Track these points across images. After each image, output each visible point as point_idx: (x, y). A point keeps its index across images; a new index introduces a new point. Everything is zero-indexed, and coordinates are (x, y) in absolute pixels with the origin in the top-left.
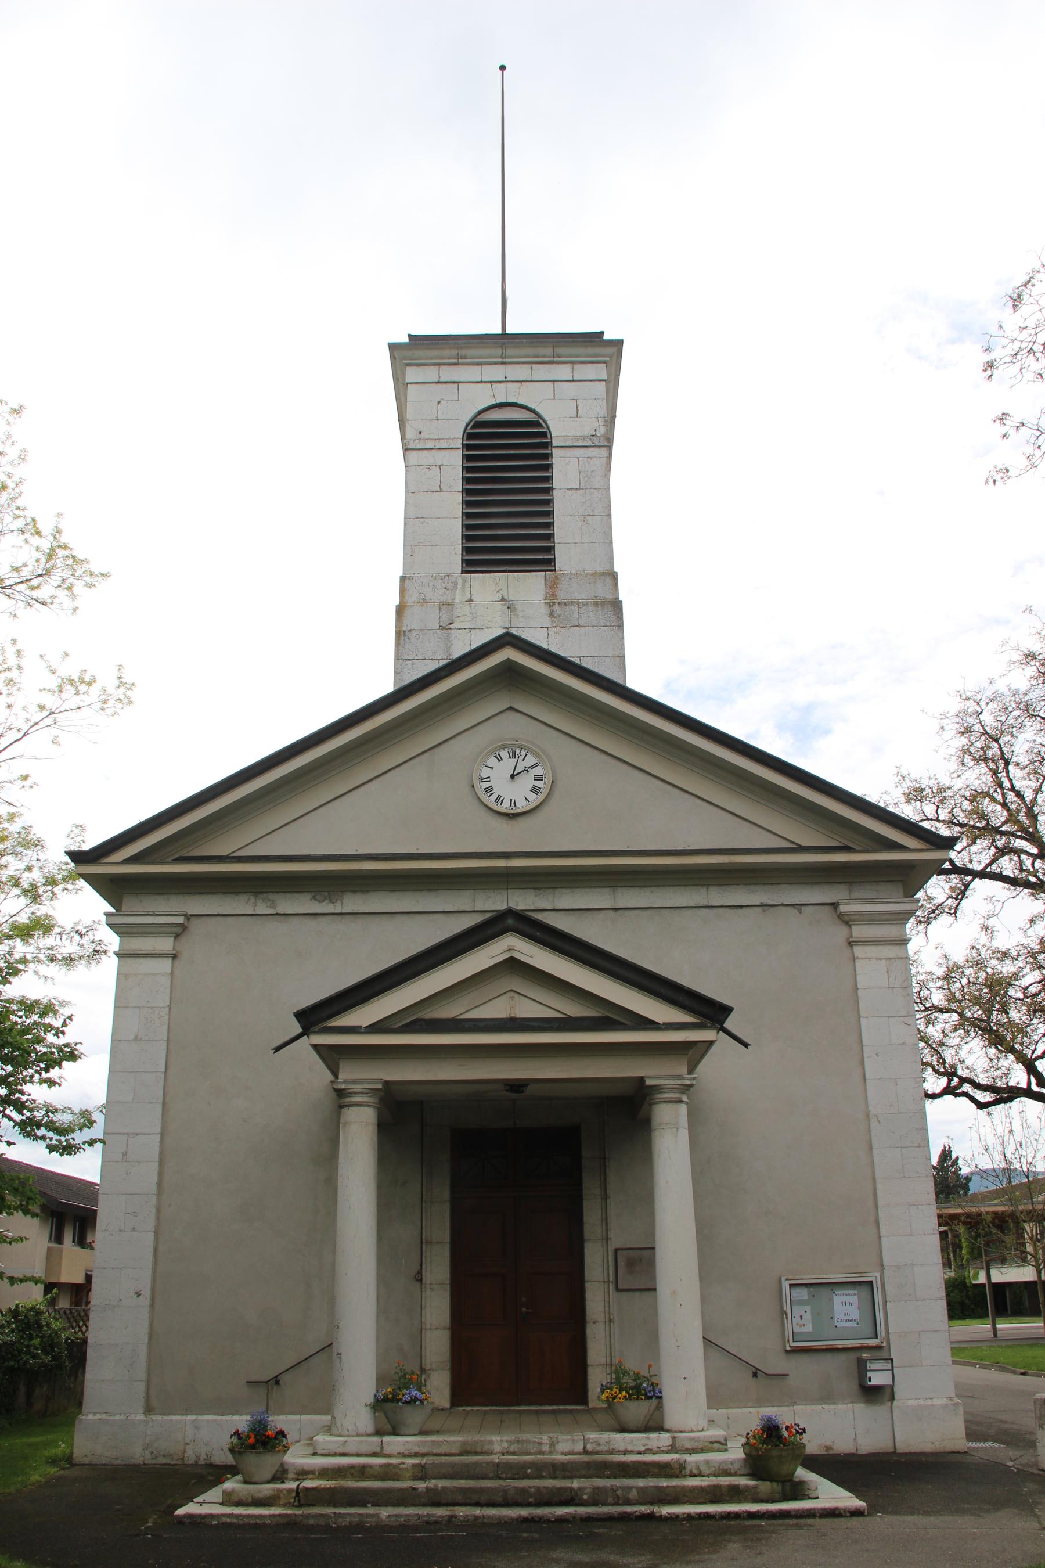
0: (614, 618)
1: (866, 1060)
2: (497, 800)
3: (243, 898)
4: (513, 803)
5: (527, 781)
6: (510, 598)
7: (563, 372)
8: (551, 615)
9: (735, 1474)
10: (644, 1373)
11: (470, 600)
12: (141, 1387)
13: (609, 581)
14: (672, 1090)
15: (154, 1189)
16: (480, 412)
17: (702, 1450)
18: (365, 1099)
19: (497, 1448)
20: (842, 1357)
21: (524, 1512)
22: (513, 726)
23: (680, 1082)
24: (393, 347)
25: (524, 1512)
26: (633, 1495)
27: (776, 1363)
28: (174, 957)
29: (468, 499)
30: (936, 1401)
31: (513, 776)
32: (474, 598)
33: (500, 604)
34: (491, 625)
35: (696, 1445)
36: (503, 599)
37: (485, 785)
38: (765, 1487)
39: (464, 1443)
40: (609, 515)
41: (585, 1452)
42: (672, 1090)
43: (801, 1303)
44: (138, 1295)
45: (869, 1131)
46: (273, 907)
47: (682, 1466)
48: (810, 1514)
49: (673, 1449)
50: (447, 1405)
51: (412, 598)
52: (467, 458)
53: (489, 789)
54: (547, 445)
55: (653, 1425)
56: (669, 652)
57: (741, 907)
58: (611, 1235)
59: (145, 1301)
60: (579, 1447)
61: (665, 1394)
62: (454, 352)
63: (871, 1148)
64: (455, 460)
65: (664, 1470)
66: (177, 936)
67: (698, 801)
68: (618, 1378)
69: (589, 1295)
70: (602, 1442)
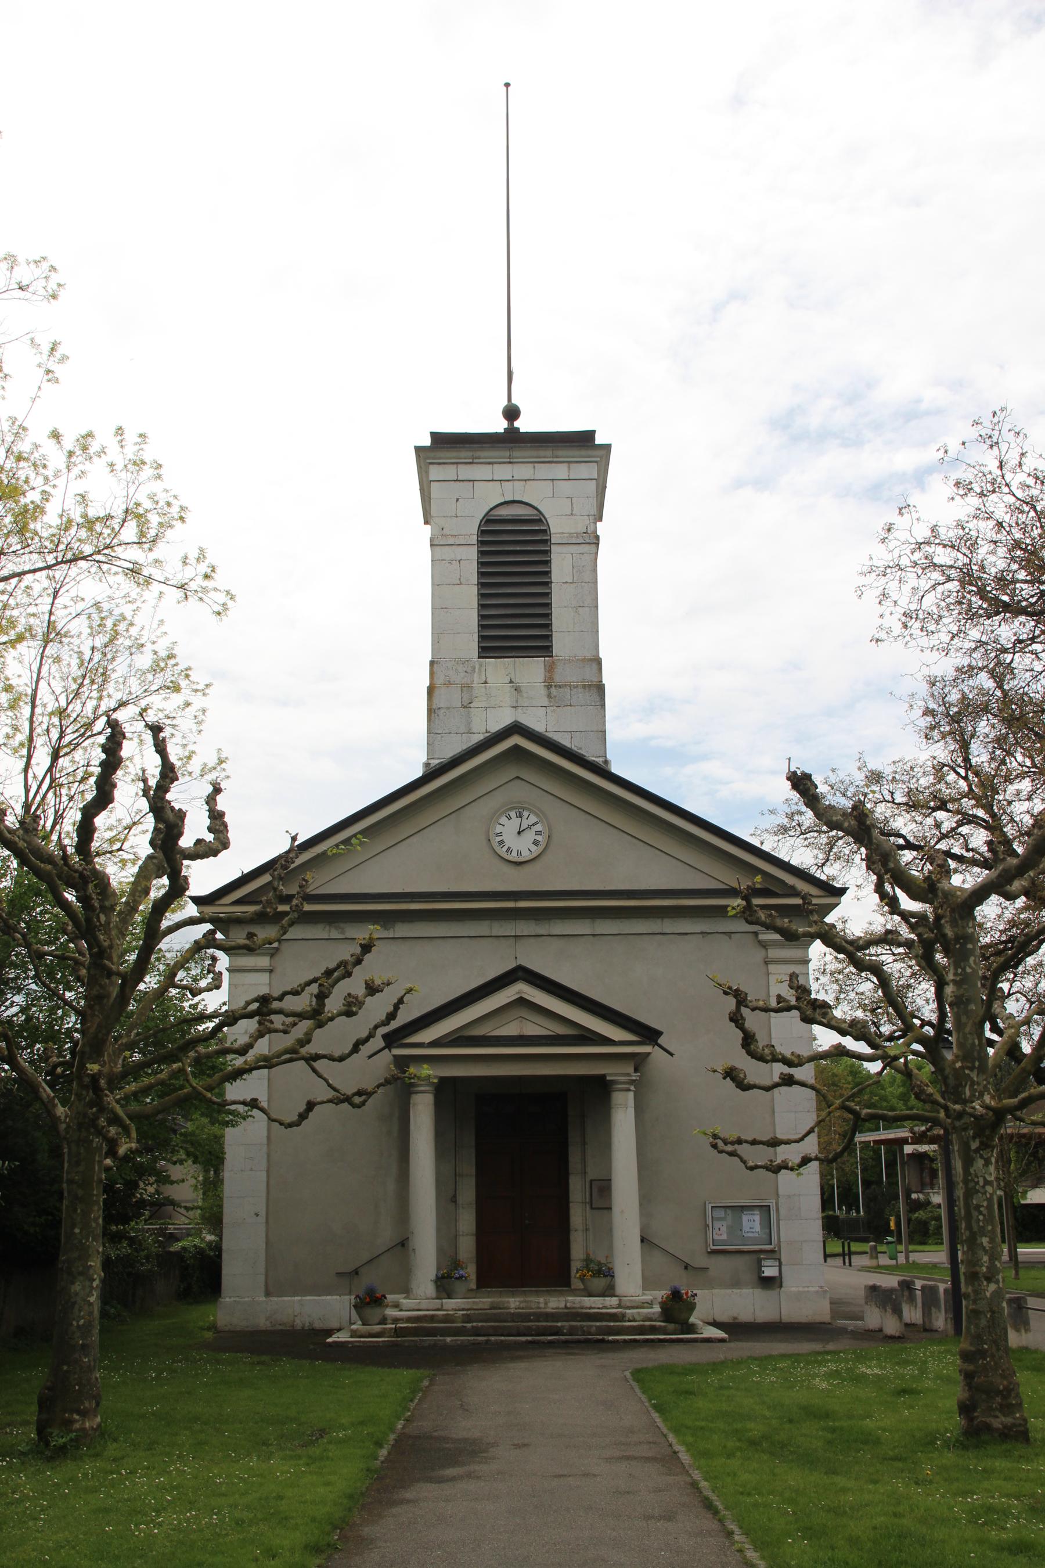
0: (598, 699)
2: (507, 851)
3: (320, 926)
4: (519, 853)
5: (530, 836)
6: (517, 680)
7: (560, 471)
8: (549, 696)
9: (655, 1321)
10: (603, 1261)
11: (486, 683)
12: (262, 1278)
13: (595, 666)
15: (265, 1141)
17: (637, 1307)
18: (427, 1088)
19: (512, 1306)
20: (747, 1257)
21: (530, 1338)
22: (518, 792)
24: (419, 450)
25: (530, 1338)
26: (593, 1329)
28: (271, 971)
29: (483, 592)
30: (811, 1289)
31: (519, 833)
32: (489, 680)
33: (510, 694)
34: (502, 704)
35: (634, 1304)
36: (511, 682)
37: (499, 839)
38: (671, 1326)
39: (492, 1303)
40: (597, 607)
41: (566, 1307)
43: (720, 1219)
44: (257, 1215)
46: (343, 933)
47: (624, 1315)
48: (695, 1340)
49: (619, 1306)
50: (474, 1287)
51: (439, 681)
52: (481, 553)
53: (502, 842)
54: (547, 542)
55: (609, 1291)
56: (635, 744)
58: (588, 1170)
59: (262, 1219)
60: (562, 1305)
61: (616, 1274)
62: (470, 454)
63: (773, 1112)
64: (472, 554)
65: (613, 1317)
67: (657, 852)
68: (587, 1265)
69: (572, 1212)
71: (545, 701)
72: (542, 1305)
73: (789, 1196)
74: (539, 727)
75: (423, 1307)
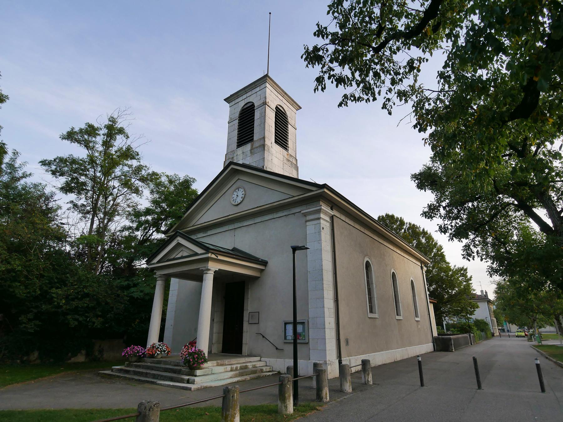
22: (239, 183)
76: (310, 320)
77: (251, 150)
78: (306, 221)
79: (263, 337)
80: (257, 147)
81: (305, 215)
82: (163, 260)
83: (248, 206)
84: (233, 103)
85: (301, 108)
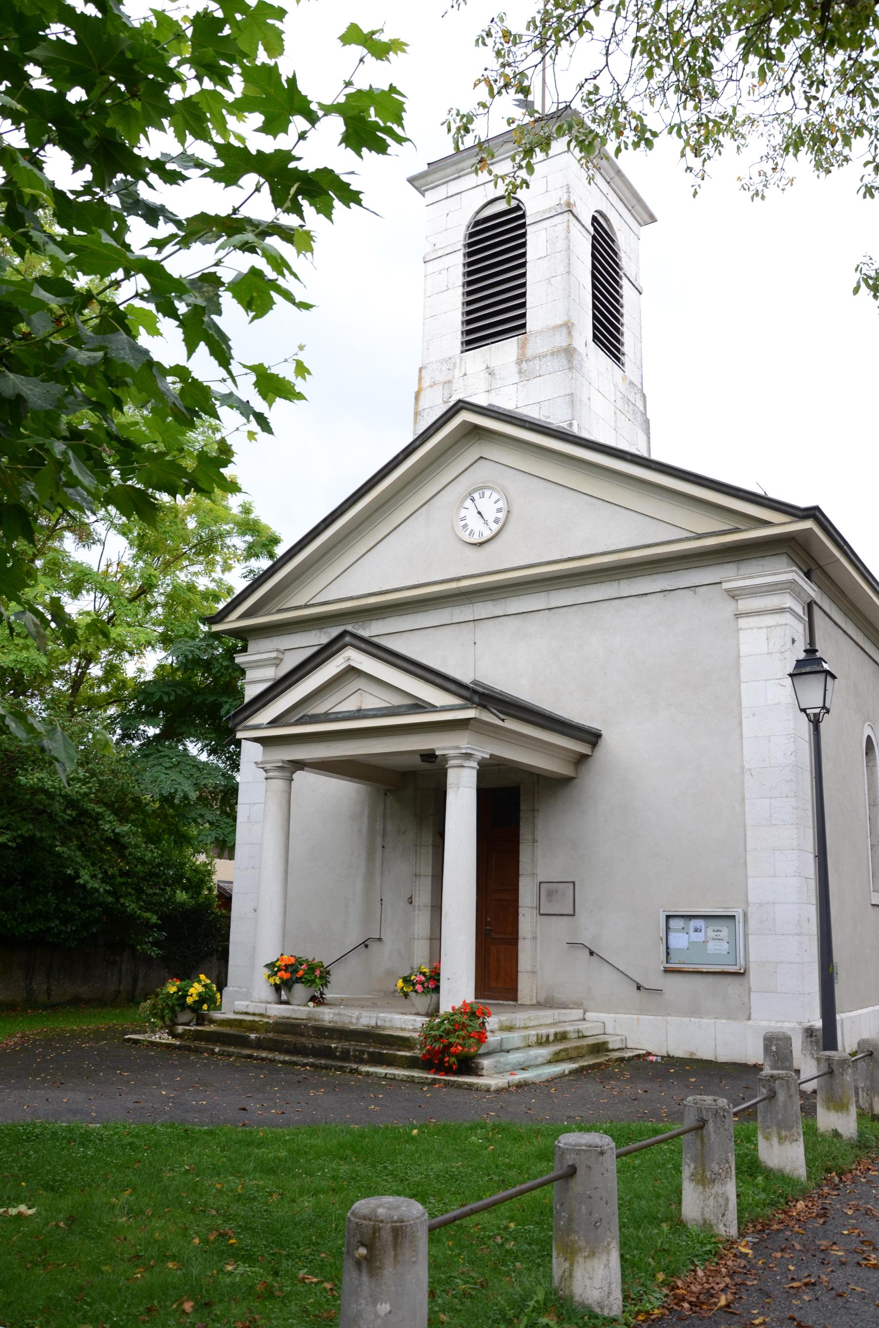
1: (744, 720)
3: (313, 633)
8: (520, 372)
11: (465, 375)
14: (455, 757)
16: (478, 213)
22: (482, 472)
23: (458, 751)
27: (654, 979)
32: (468, 373)
36: (488, 368)
37: (463, 523)
42: (455, 757)
45: (743, 784)
53: (465, 526)
57: (646, 594)
62: (454, 168)
63: (744, 799)
66: (277, 665)
67: (618, 508)
70: (387, 1020)
71: (516, 378)
72: (354, 1021)
73: (761, 905)
74: (482, 400)
75: (251, 1011)
76: (751, 910)
77: (519, 362)
78: (738, 616)
79: (592, 953)
80: (540, 357)
81: (734, 595)
82: (284, 720)
83: (517, 555)
84: (441, 192)
85: (653, 219)
